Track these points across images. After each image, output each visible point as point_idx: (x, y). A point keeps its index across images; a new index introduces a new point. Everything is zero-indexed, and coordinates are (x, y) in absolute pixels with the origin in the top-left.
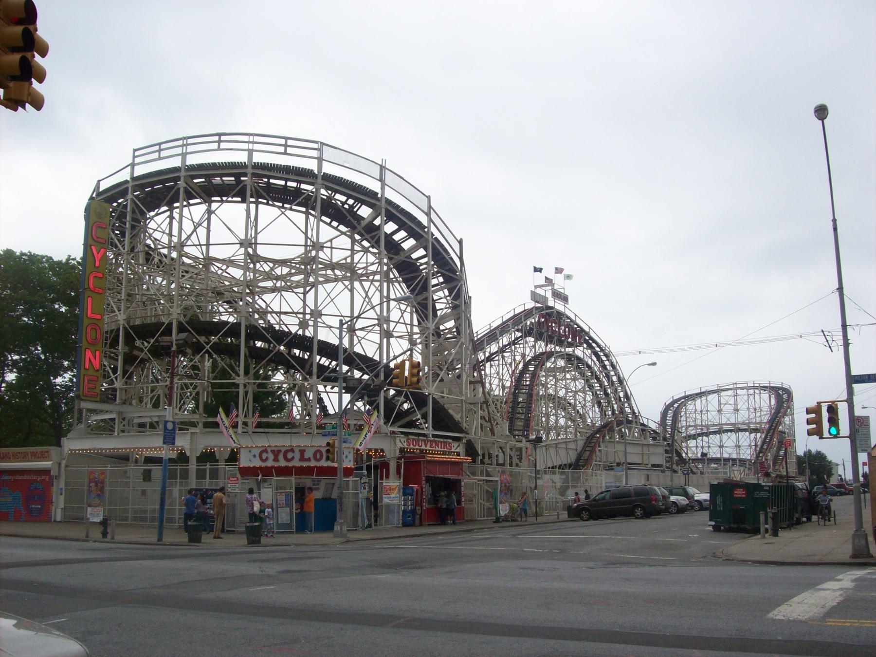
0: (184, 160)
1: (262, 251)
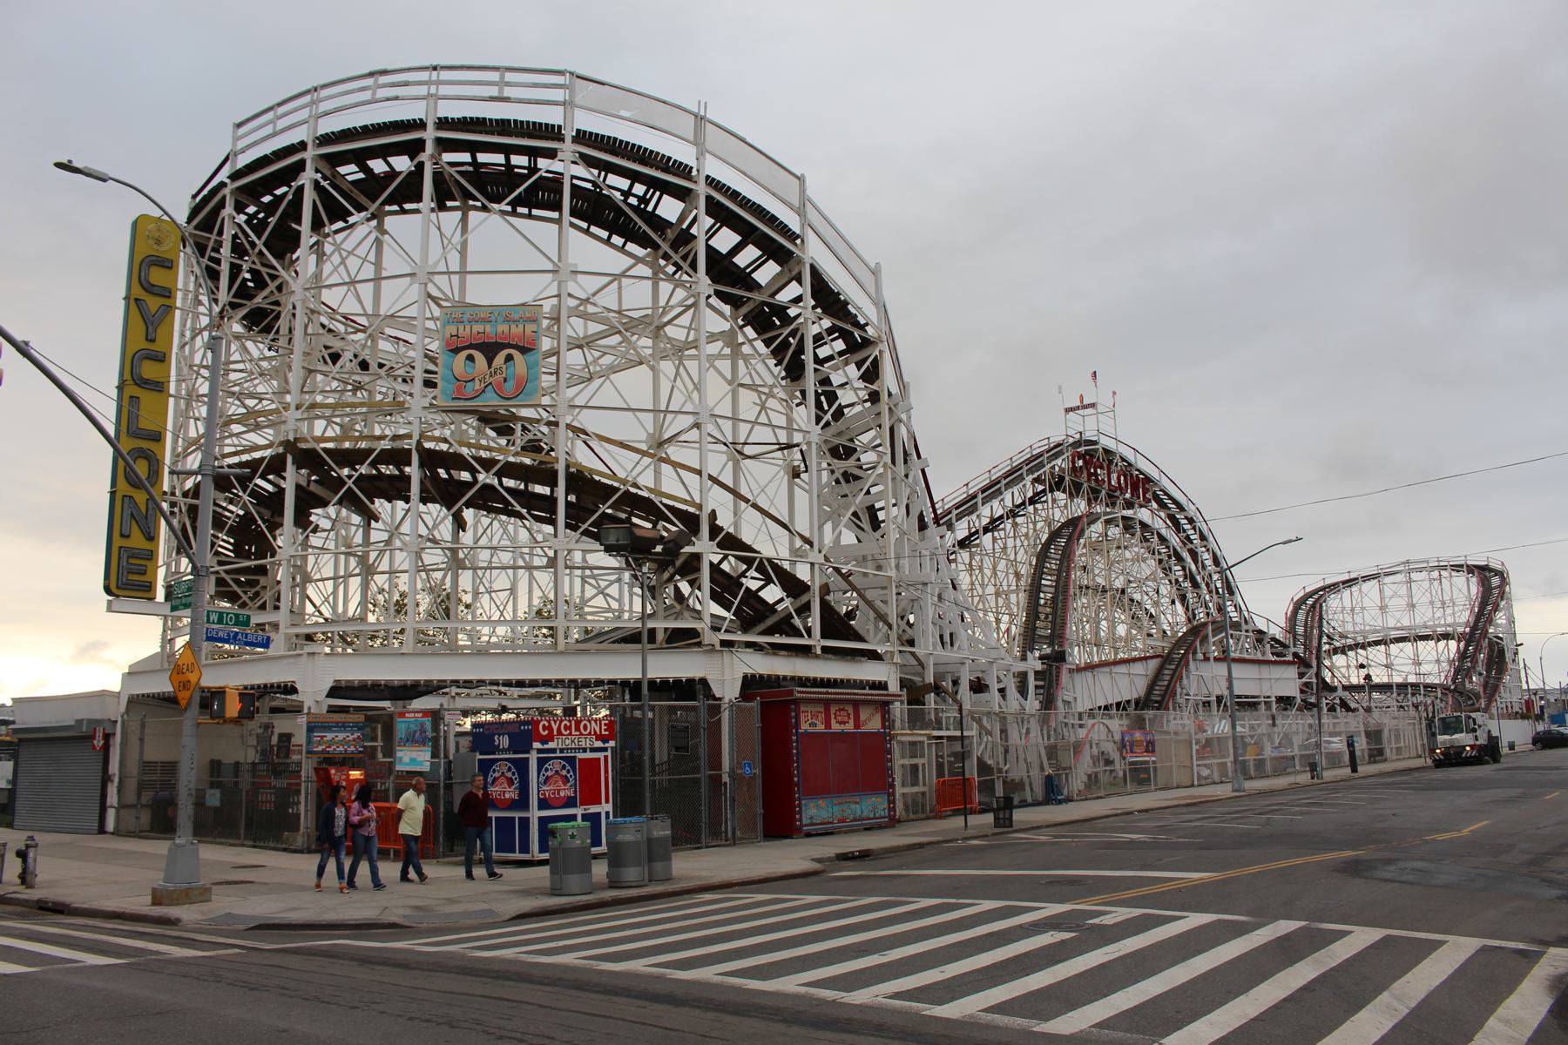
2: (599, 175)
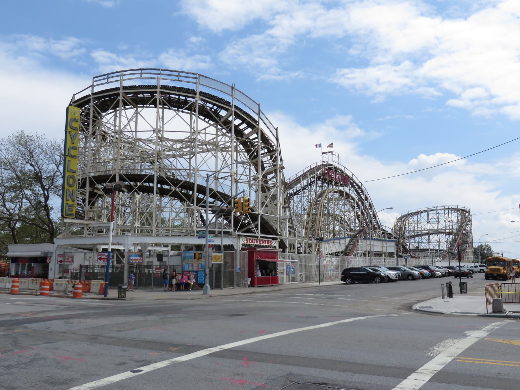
0: (121, 83)
1: (166, 135)
2: (205, 103)
